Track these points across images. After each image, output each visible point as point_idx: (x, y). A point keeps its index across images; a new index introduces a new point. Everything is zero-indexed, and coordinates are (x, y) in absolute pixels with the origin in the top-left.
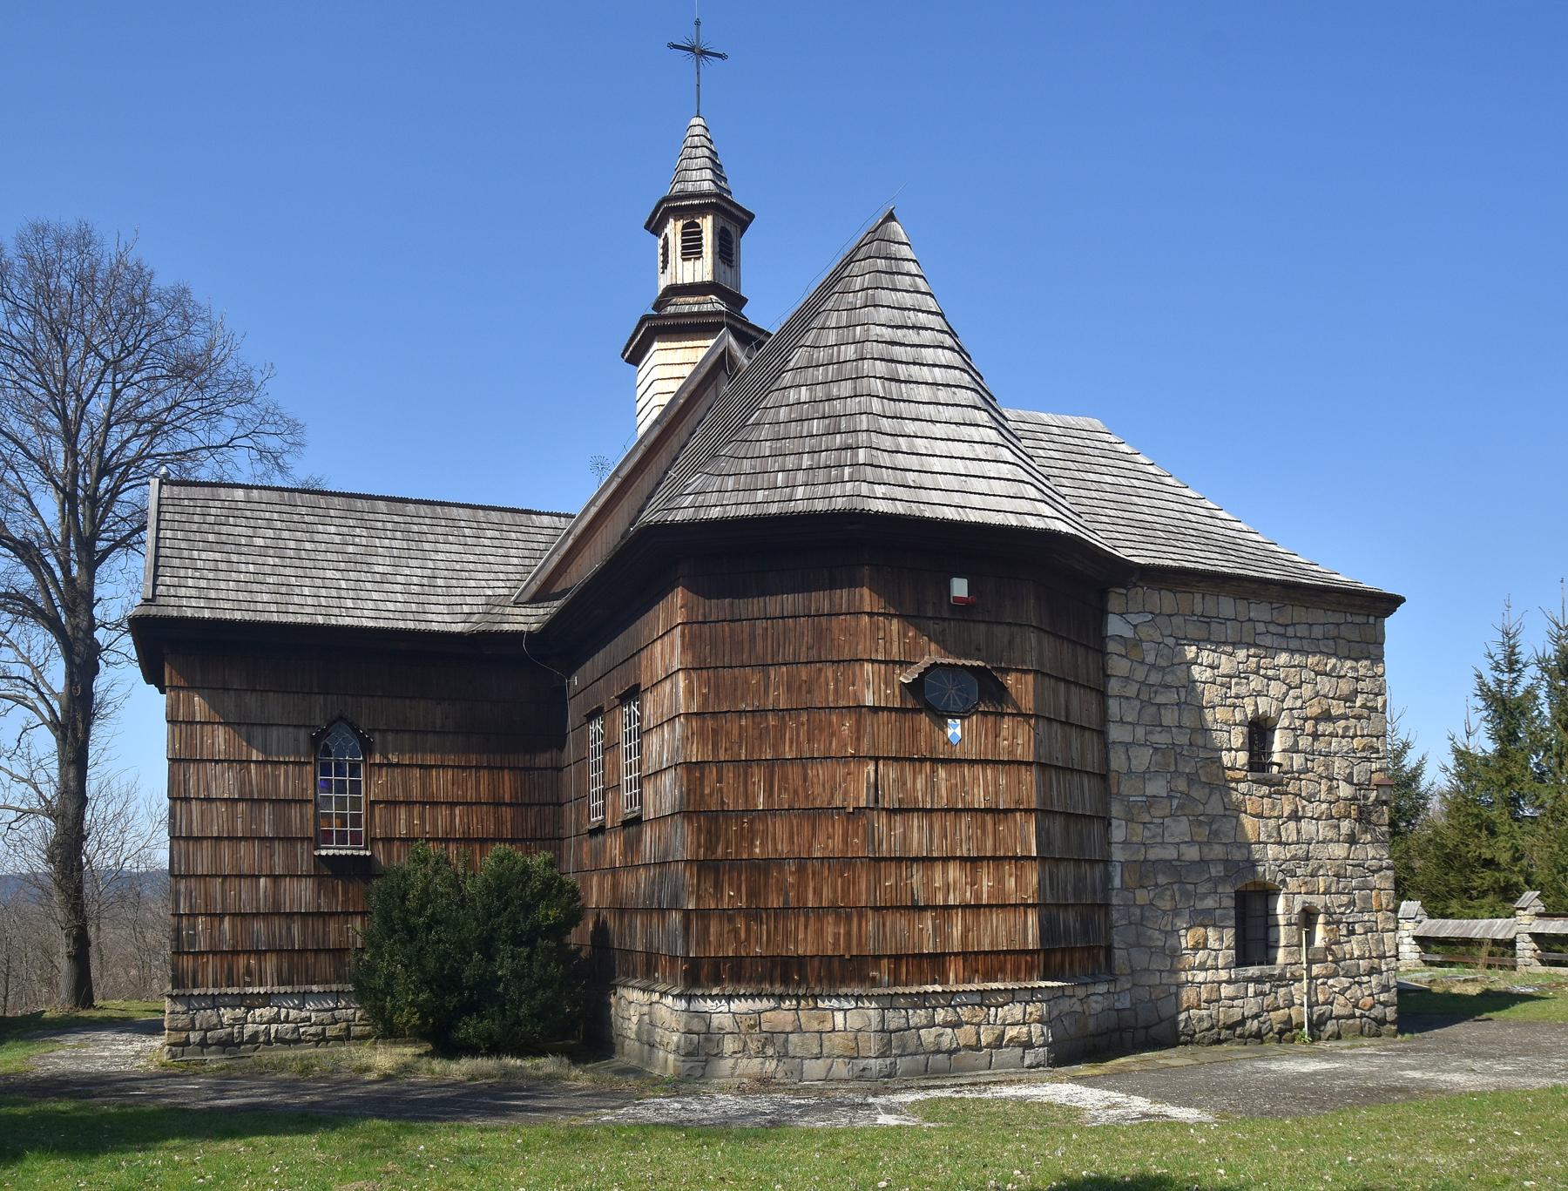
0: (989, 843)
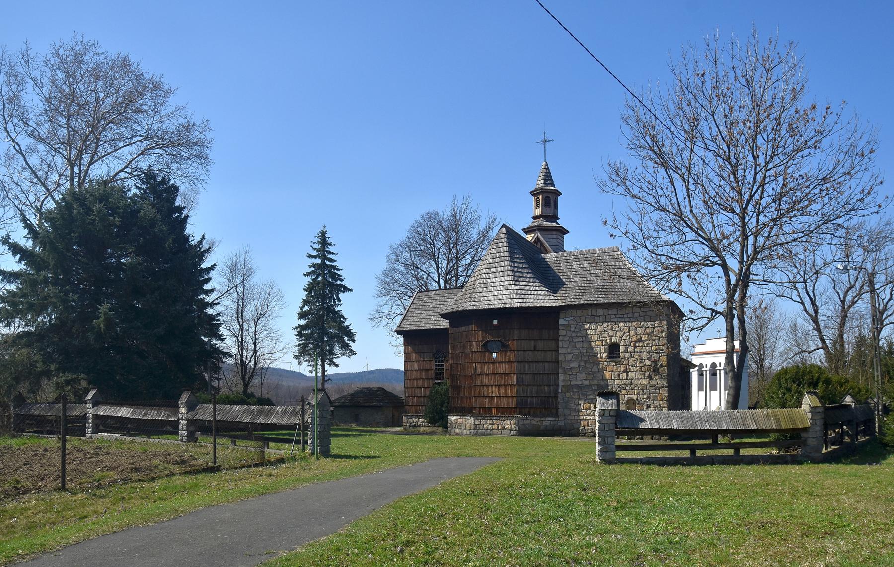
0: (503, 381)
